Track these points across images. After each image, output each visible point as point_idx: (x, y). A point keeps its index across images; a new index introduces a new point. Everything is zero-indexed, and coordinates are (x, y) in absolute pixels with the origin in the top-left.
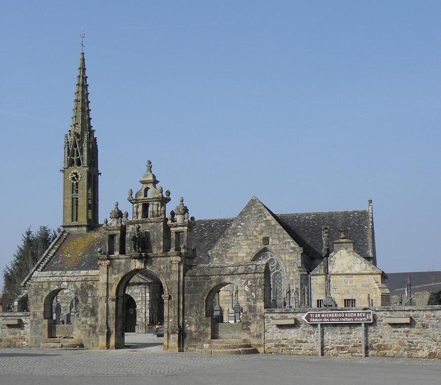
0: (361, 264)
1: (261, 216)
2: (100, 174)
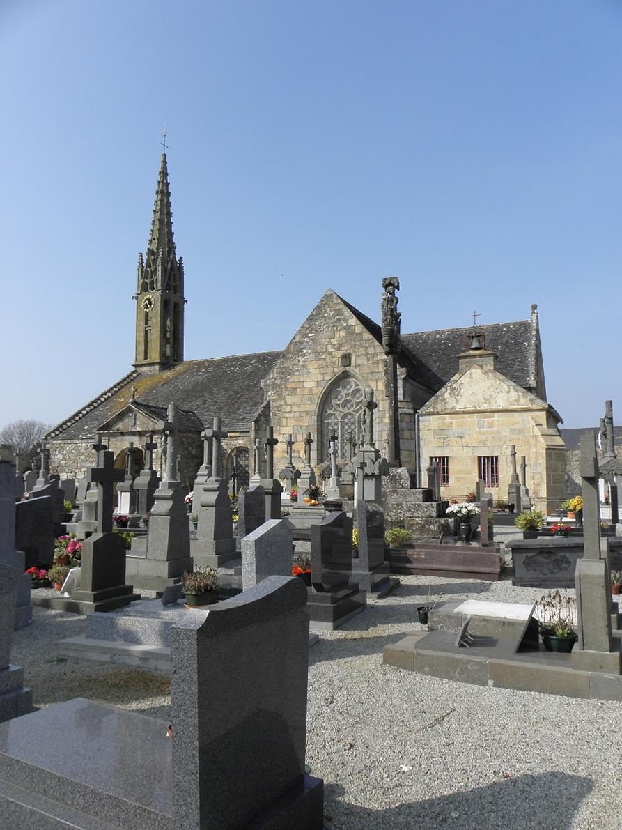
0: (508, 392)
1: (339, 320)
2: (186, 301)
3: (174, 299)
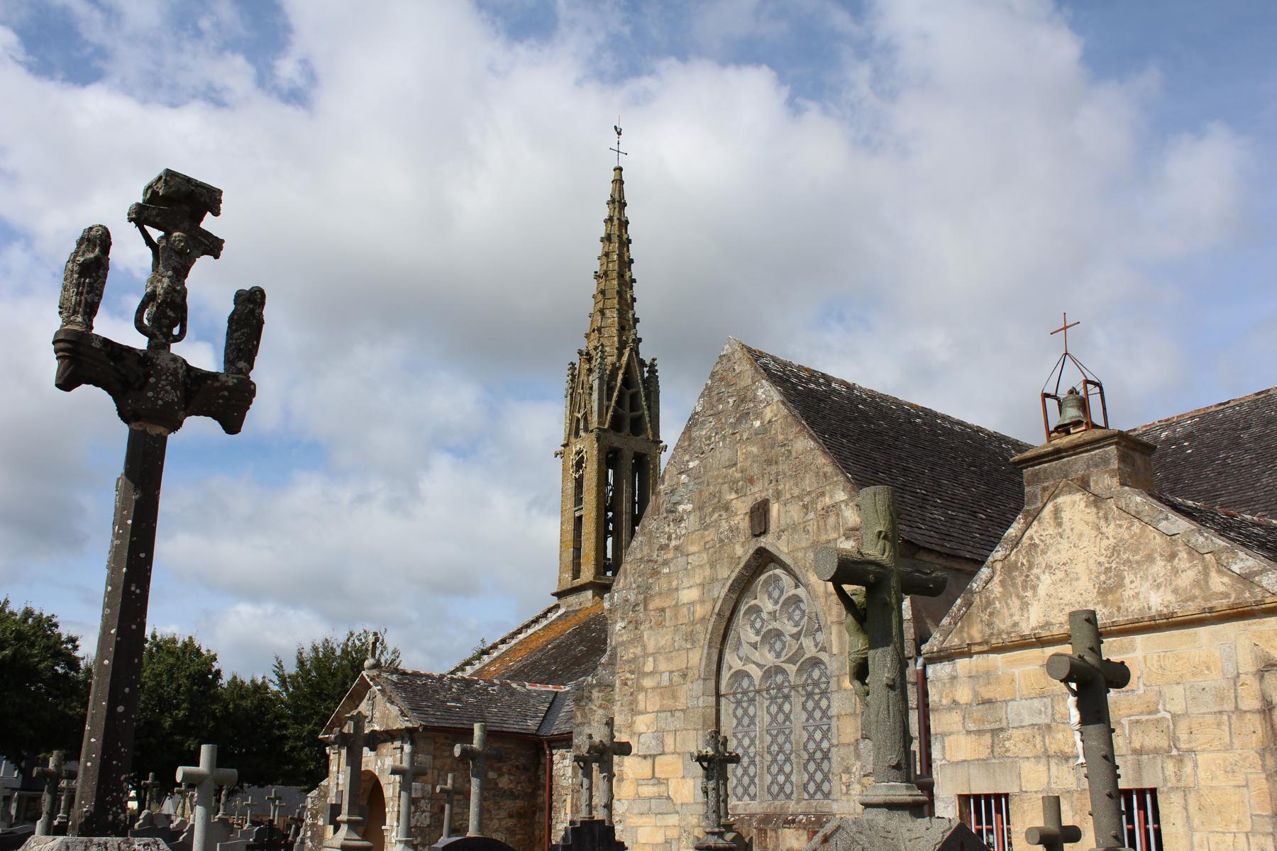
3: (628, 444)
